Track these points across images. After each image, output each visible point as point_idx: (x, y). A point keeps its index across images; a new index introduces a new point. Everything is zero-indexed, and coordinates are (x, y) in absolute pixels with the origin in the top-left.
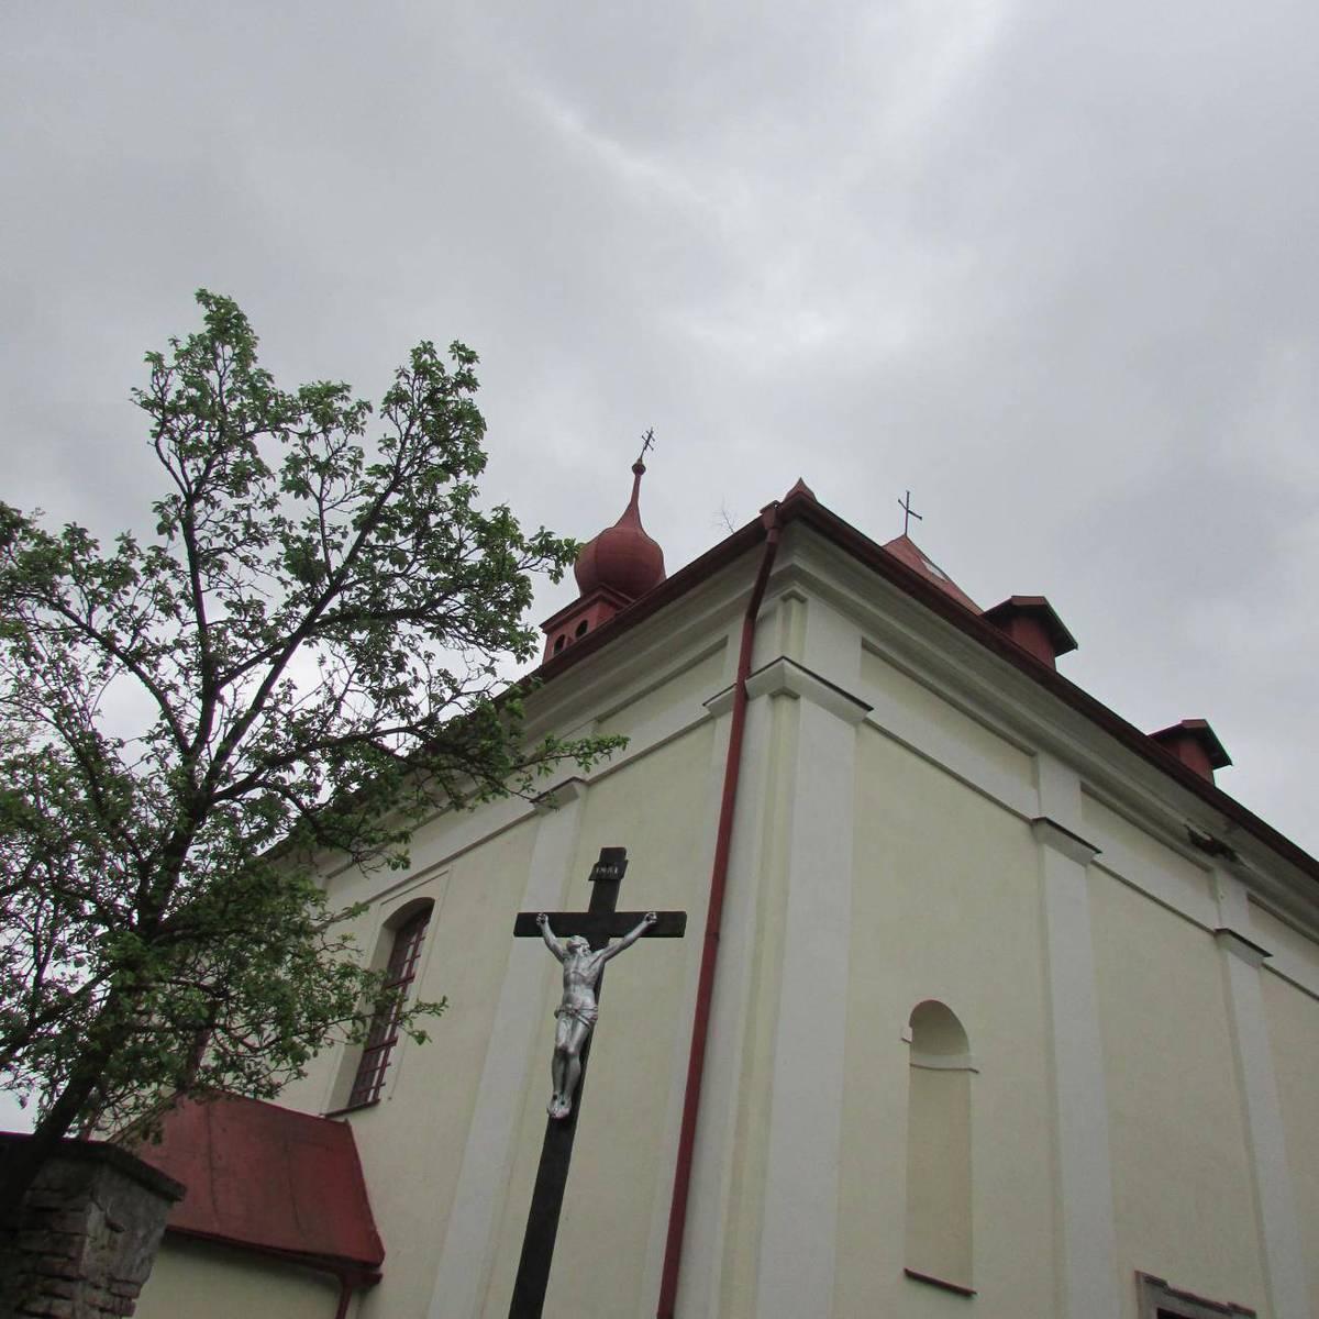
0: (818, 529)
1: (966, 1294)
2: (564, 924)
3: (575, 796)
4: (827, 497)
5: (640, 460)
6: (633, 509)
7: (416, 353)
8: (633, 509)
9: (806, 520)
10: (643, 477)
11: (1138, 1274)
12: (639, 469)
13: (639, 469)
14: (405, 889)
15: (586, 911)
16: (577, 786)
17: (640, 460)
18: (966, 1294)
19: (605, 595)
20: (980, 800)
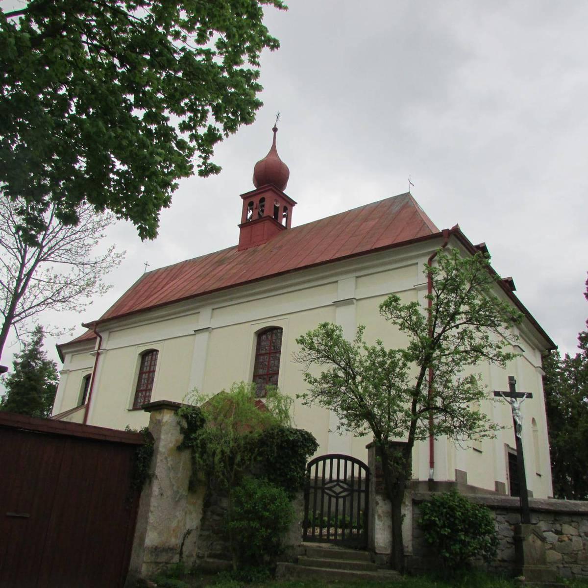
0: (458, 238)
1: (480, 452)
2: (506, 394)
3: (353, 303)
4: (464, 230)
5: (275, 125)
6: (274, 148)
7: (275, 41)
8: (274, 148)
9: (455, 235)
10: (277, 133)
11: (505, 444)
12: (275, 130)
13: (275, 130)
14: (266, 320)
15: (517, 391)
16: (354, 301)
17: (275, 125)
18: (480, 452)
19: (273, 188)
20: (368, 300)
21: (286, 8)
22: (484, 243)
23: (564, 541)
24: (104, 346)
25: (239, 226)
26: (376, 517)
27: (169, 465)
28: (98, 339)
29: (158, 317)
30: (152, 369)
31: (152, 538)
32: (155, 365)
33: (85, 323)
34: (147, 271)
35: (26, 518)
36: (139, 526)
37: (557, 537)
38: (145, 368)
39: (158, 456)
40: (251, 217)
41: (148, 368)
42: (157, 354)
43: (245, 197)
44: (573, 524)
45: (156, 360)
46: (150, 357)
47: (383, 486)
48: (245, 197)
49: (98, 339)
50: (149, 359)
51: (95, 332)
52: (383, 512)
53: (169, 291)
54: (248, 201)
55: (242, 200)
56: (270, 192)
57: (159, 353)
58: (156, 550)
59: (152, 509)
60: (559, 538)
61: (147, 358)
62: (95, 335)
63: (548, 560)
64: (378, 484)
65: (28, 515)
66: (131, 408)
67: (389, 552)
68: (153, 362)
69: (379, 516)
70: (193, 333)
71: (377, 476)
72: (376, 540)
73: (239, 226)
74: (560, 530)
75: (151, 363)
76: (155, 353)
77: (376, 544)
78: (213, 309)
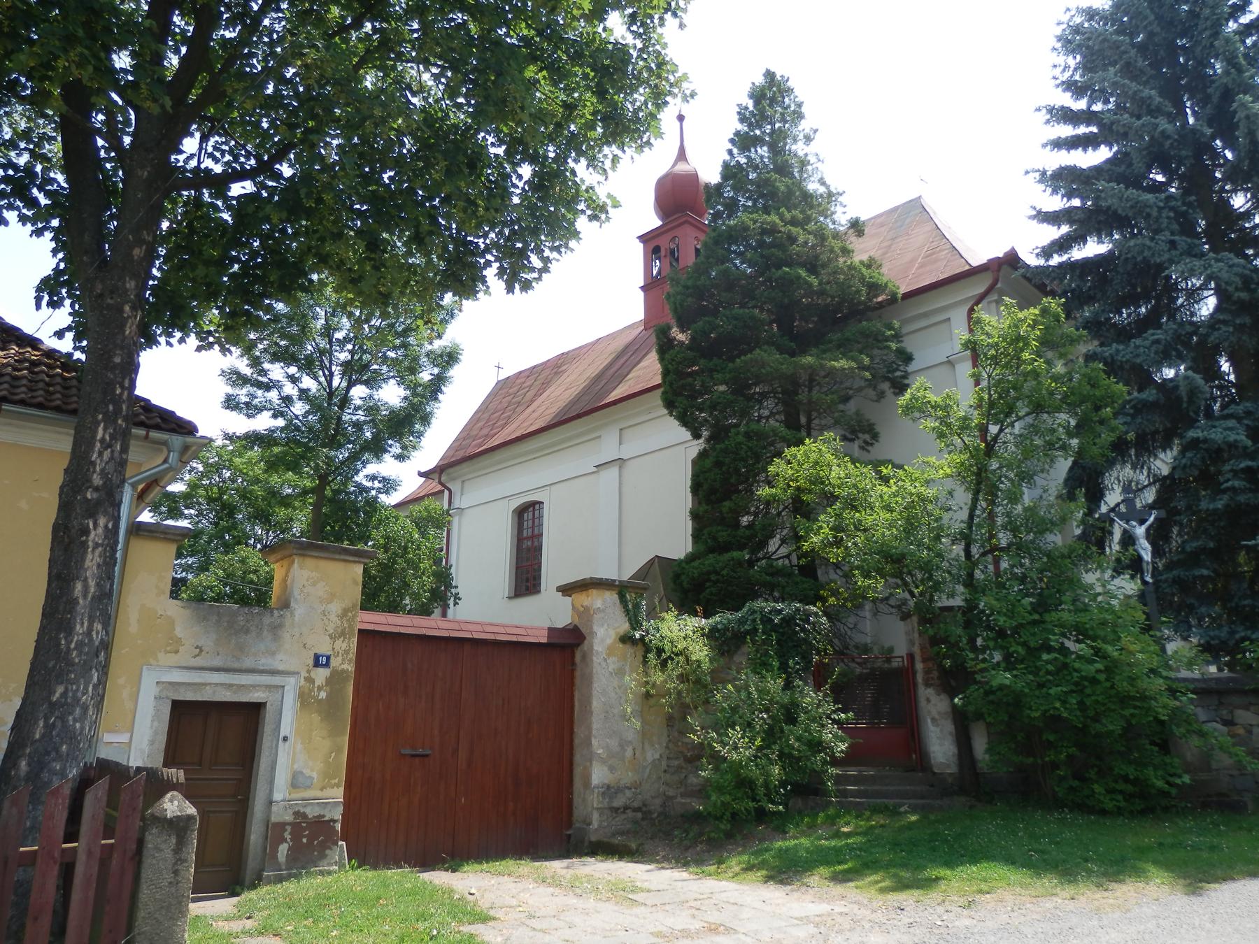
10: (684, 123)
21: (1044, 146)
22: (1013, 248)
23: (1239, 735)
24: (456, 504)
25: (642, 288)
26: (929, 721)
27: (610, 670)
28: (446, 492)
29: (532, 452)
30: (536, 532)
31: (599, 775)
32: (541, 525)
33: (423, 470)
34: (502, 377)
35: (427, 756)
36: (578, 758)
37: (1225, 729)
38: (525, 532)
39: (595, 658)
40: (659, 273)
41: (530, 530)
42: (541, 509)
43: (644, 238)
44: (1252, 708)
45: (541, 517)
46: (531, 514)
47: (935, 674)
48: (644, 238)
49: (446, 492)
50: (530, 517)
51: (440, 483)
52: (939, 713)
53: (543, 408)
54: (652, 245)
55: (642, 245)
56: (686, 226)
57: (546, 507)
58: (610, 791)
59: (594, 732)
60: (1229, 731)
61: (526, 515)
62: (439, 488)
63: (1214, 765)
64: (927, 672)
65: (428, 752)
66: (513, 595)
67: (953, 769)
68: (537, 521)
69: (933, 720)
70: (595, 469)
71: (924, 661)
72: (932, 755)
73: (642, 288)
74: (1230, 718)
75: (533, 522)
76: (537, 506)
77: (933, 762)
78: (621, 430)
